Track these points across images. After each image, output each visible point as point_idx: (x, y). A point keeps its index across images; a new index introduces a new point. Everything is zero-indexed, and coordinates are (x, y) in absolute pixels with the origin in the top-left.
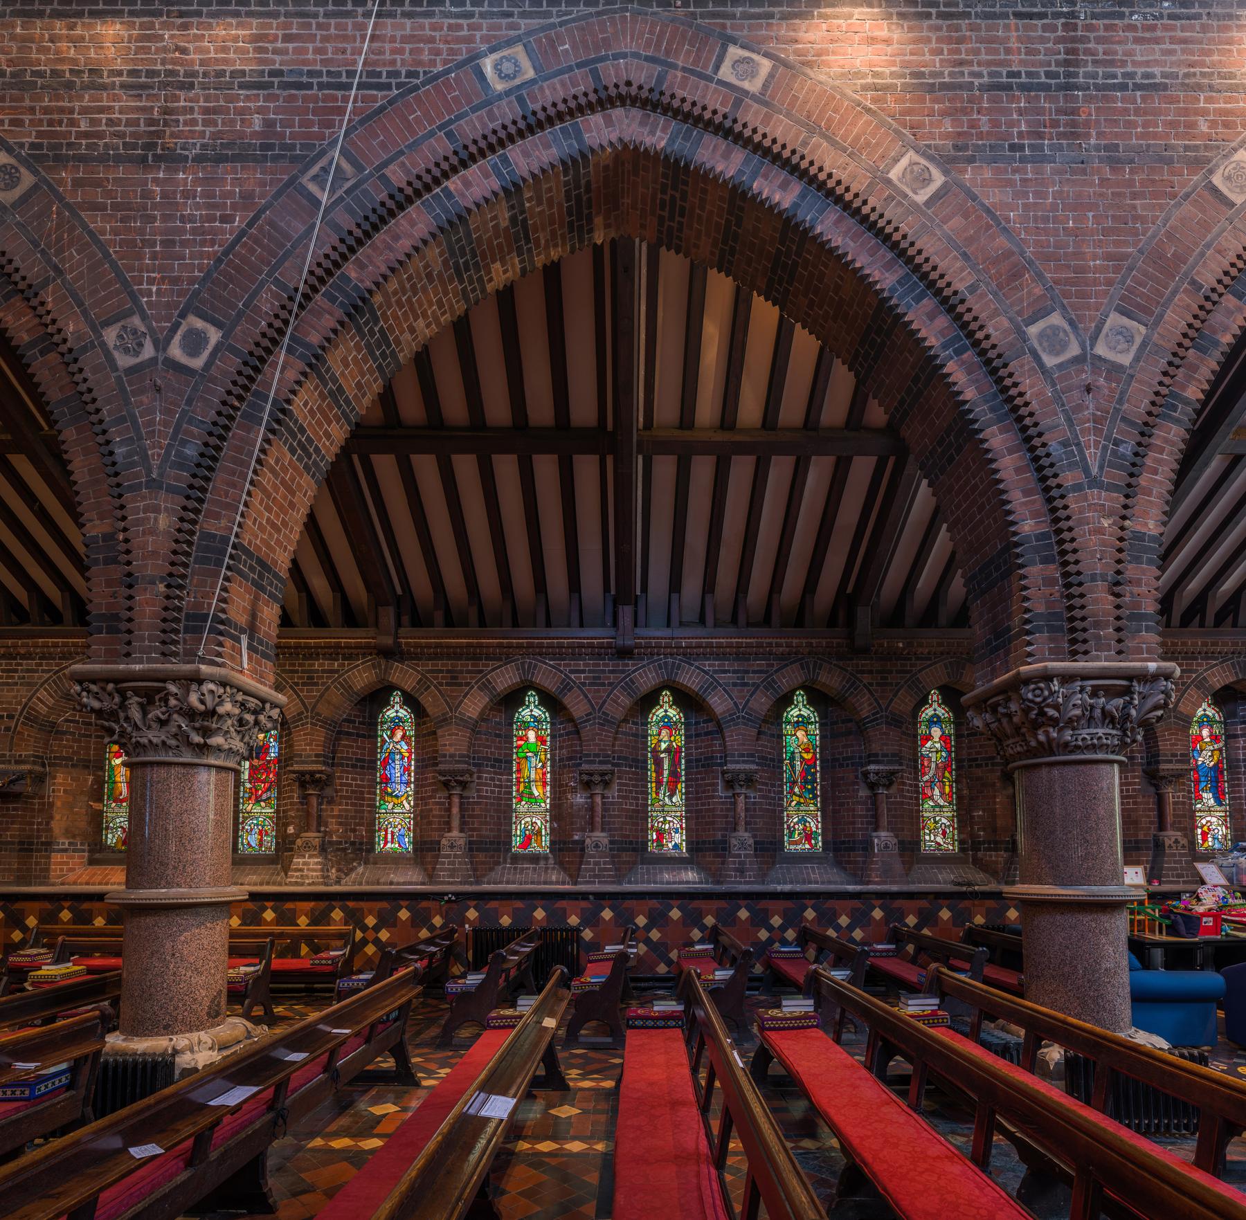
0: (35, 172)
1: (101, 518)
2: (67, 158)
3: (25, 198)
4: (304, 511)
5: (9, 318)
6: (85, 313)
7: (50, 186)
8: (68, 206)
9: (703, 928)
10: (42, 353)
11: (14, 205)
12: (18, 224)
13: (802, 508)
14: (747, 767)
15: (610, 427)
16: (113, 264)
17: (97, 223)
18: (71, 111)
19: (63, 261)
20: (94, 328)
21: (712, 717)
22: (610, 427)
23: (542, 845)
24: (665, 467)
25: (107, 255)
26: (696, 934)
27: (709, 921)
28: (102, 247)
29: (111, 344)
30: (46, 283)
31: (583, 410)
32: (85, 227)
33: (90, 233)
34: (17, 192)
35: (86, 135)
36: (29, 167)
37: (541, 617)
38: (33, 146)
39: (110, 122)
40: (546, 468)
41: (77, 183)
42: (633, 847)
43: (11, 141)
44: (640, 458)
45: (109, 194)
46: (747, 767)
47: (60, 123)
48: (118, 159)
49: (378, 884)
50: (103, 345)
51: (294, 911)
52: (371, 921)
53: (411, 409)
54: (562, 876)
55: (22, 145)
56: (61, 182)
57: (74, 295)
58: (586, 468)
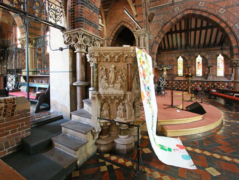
0: (225, 10)
1: (235, 44)
2: (230, 7)
3: (224, 13)
4: (160, 41)
5: (222, 25)
6: (233, 23)
7: (228, 11)
8: (230, 12)
9: (199, 85)
10: (226, 28)
11: (223, 14)
12: (224, 15)
13: (202, 35)
14: (190, 65)
15: (186, 29)
16: (236, 17)
17: (234, 13)
18: (230, 2)
19: (230, 18)
20: (234, 24)
21: (186, 59)
22: (186, 29)
23: (201, 75)
24: (193, 33)
25: (235, 17)
26: (199, 86)
27: (200, 84)
28: (235, 16)
29: (236, 26)
30: (228, 21)
31: (183, 28)
32: (232, 14)
33: (233, 15)
34: (223, 12)
35: (232, 4)
36: (225, 9)
37: (177, 49)
38: (225, 7)
39: (235, 2)
40: (178, 35)
41: (231, 10)
42: (194, 75)
43: (222, 7)
44: (190, 32)
45: (235, 10)
46: (190, 65)
47: (228, 4)
48: (236, 6)
49: (220, 80)
50: (235, 26)
51: (230, 84)
52: (221, 85)
53: (174, 30)
54: (204, 79)
55: (224, 7)
56: (229, 10)
57: (231, 22)
58: (183, 34)
